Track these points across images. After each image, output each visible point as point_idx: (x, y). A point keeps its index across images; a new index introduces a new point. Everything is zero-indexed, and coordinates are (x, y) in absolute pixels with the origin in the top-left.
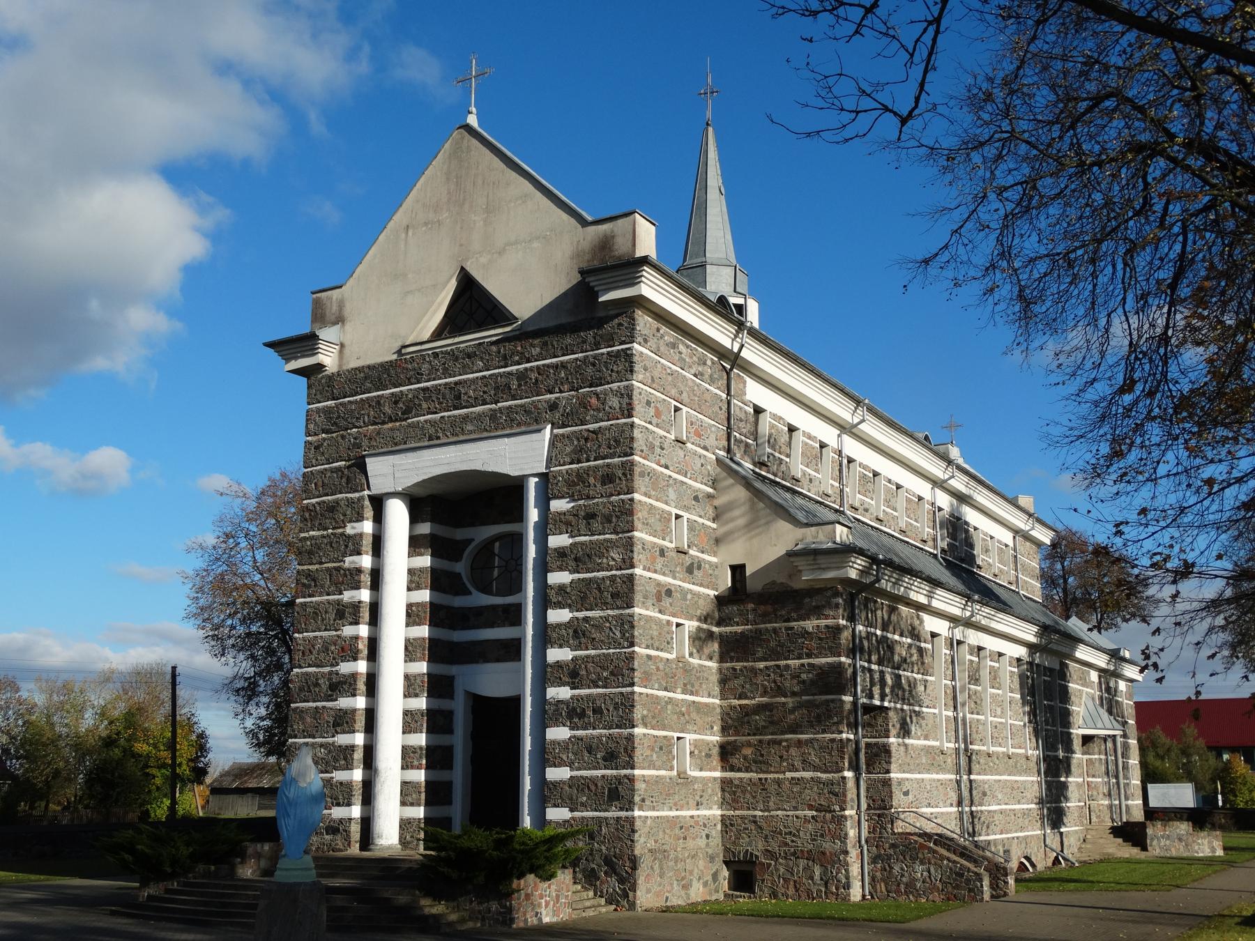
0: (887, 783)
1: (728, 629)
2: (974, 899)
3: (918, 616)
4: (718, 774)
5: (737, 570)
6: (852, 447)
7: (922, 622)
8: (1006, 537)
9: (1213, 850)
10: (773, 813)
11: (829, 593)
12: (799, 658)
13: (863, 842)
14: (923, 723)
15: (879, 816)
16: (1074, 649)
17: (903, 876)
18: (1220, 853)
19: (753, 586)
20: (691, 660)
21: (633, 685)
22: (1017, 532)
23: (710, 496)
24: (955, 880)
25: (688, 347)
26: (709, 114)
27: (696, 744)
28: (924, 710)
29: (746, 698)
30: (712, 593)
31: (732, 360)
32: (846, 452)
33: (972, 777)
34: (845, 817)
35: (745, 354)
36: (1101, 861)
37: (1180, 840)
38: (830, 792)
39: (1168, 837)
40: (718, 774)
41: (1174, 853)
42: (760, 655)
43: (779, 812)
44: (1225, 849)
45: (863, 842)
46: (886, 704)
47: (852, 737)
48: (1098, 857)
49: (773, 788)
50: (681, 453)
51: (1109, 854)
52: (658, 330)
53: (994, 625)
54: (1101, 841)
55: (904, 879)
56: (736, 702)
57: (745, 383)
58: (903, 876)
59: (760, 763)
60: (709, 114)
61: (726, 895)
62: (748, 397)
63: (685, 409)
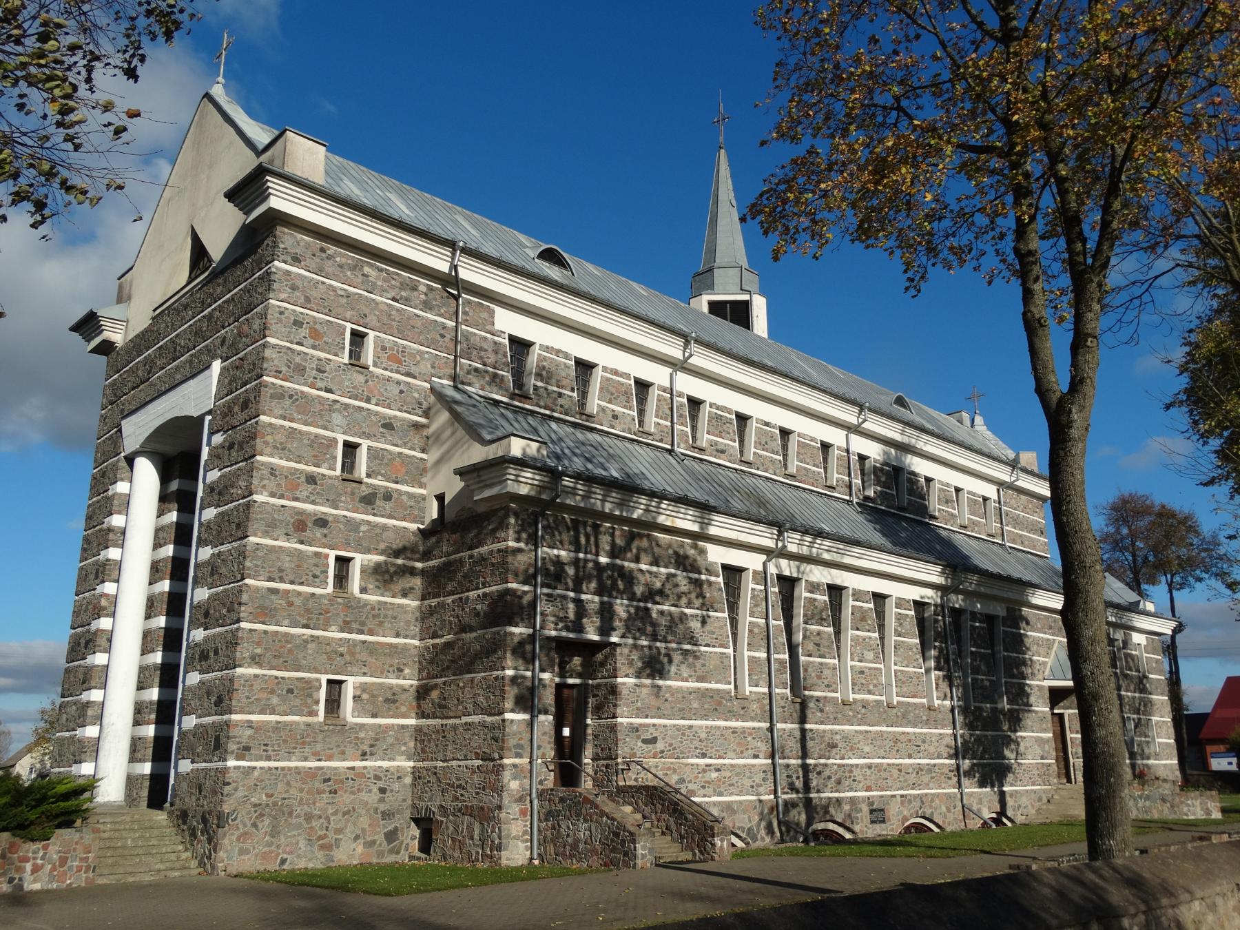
0: (613, 729)
1: (430, 563)
2: (626, 864)
3: (695, 547)
4: (412, 722)
5: (440, 498)
6: (688, 385)
7: (703, 552)
8: (991, 491)
9: (1208, 812)
10: (451, 763)
11: (501, 514)
12: (477, 589)
13: (534, 795)
14: (698, 663)
15: (607, 766)
16: (1023, 593)
17: (568, 836)
18: (1217, 815)
19: (450, 515)
20: (364, 596)
21: (238, 621)
22: (1000, 484)
23: (417, 426)
24: (612, 841)
25: (381, 270)
26: (722, 139)
27: (364, 688)
28: (703, 649)
29: (438, 637)
30: (414, 526)
31: (450, 282)
32: (678, 387)
33: (808, 726)
34: (502, 766)
35: (464, 274)
36: (1061, 824)
37: (1164, 800)
38: (492, 738)
39: (1148, 798)
40: (412, 722)
41: (1156, 816)
42: (449, 588)
43: (455, 763)
44: (1224, 811)
45: (534, 795)
46: (614, 639)
47: (529, 674)
48: (1056, 819)
49: (450, 735)
50: (362, 379)
51: (1072, 817)
52: (323, 250)
53: (847, 560)
54: (1071, 801)
55: (570, 840)
56: (431, 642)
57: (492, 313)
58: (568, 836)
59: (442, 709)
60: (722, 139)
61: (411, 858)
62: (497, 327)
63: (372, 334)
